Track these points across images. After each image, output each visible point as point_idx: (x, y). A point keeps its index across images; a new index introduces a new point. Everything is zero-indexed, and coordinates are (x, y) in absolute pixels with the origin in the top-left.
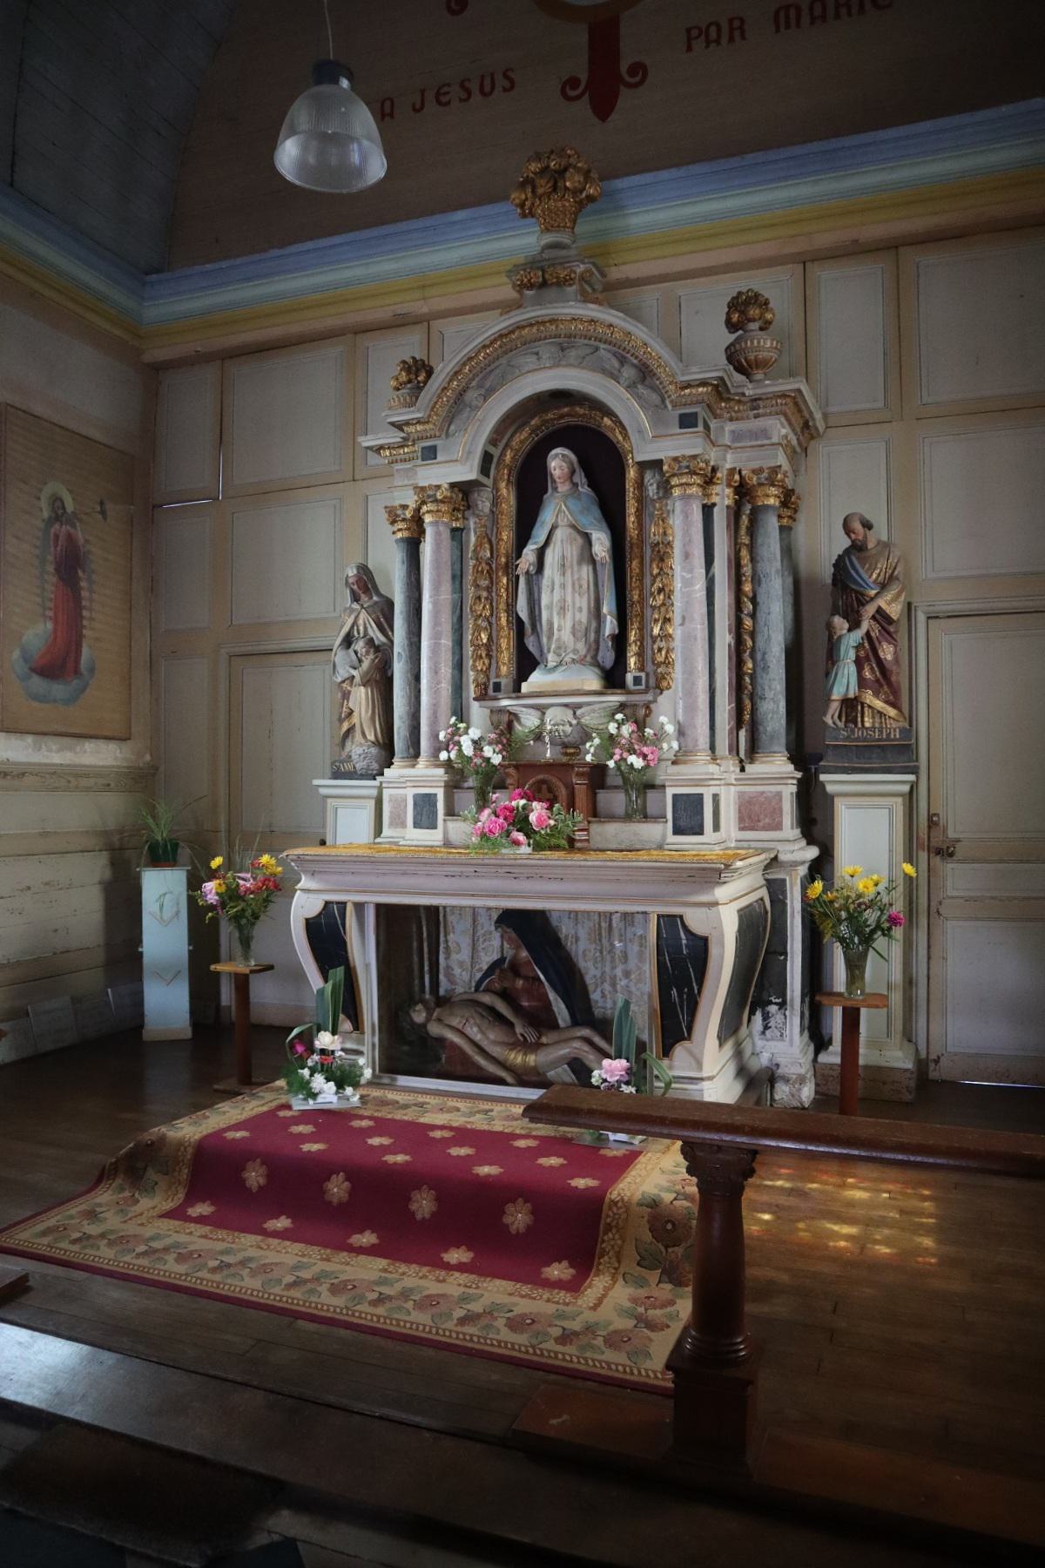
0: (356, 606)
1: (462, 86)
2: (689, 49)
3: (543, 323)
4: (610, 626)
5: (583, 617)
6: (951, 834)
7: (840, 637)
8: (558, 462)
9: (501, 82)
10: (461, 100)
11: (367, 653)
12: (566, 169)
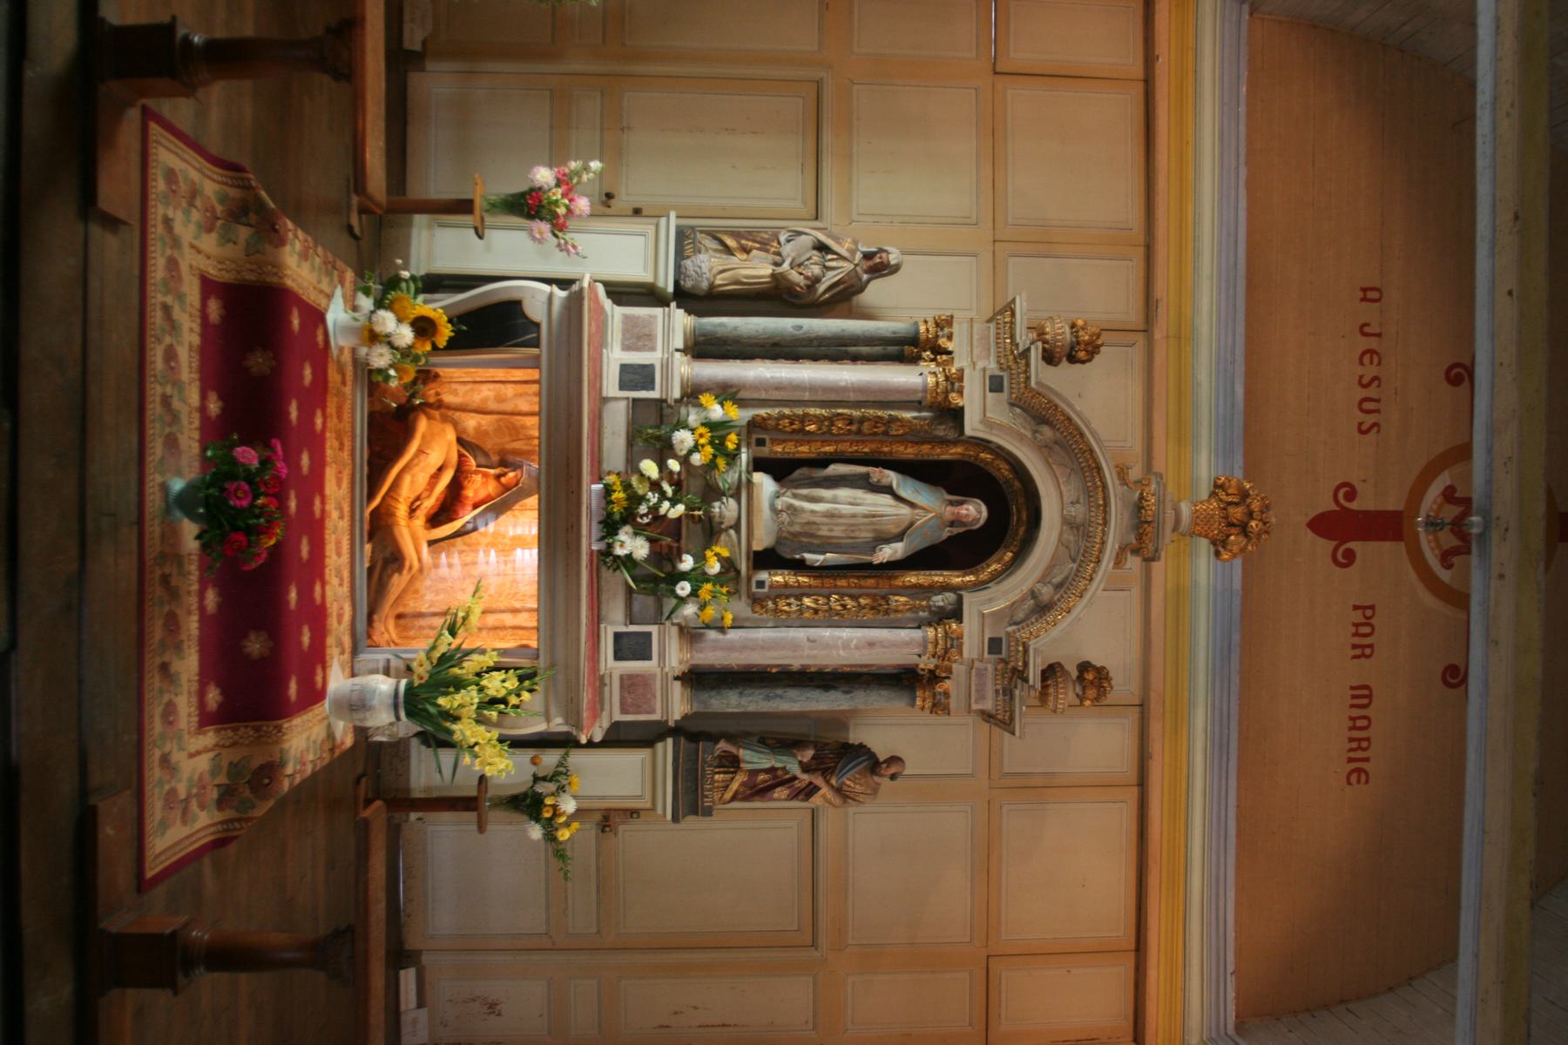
0: (859, 256)
1: (1375, 378)
2: (1356, 608)
3: (1105, 512)
5: (824, 532)
6: (621, 828)
7: (794, 756)
8: (974, 511)
9: (1369, 420)
11: (807, 278)
12: (1246, 536)
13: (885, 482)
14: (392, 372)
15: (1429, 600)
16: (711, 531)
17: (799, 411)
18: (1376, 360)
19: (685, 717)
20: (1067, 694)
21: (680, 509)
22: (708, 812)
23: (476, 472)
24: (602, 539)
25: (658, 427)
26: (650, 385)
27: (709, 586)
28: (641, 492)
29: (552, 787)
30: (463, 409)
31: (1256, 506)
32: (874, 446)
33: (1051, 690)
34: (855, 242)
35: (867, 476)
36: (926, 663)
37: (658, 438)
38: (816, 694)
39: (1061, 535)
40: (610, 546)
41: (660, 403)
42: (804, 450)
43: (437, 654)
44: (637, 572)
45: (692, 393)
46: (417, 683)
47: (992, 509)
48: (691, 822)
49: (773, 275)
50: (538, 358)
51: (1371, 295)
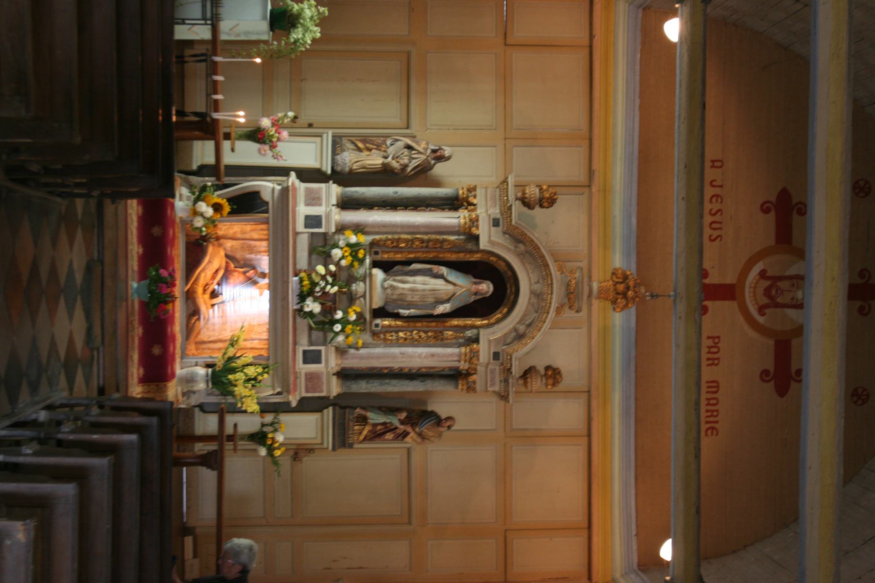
0: (429, 151)
4: (404, 312)
5: (409, 298)
6: (304, 459)
8: (486, 287)
9: (716, 233)
13: (440, 272)
14: (204, 229)
15: (752, 333)
16: (352, 299)
17: (396, 236)
18: (719, 200)
19: (339, 396)
20: (536, 383)
21: (336, 288)
22: (351, 446)
23: (236, 271)
24: (298, 303)
25: (324, 246)
26: (319, 225)
27: (350, 326)
28: (317, 281)
29: (270, 429)
30: (225, 237)
31: (631, 284)
32: (435, 254)
33: (529, 380)
34: (427, 144)
35: (430, 270)
36: (463, 366)
37: (324, 252)
38: (406, 382)
39: (530, 299)
40: (302, 307)
41: (325, 235)
42: (399, 257)
43: (226, 356)
44: (314, 320)
45: (341, 228)
46: (218, 369)
47: (495, 288)
48: (343, 453)
49: (383, 164)
50: (268, 218)
51: (717, 164)
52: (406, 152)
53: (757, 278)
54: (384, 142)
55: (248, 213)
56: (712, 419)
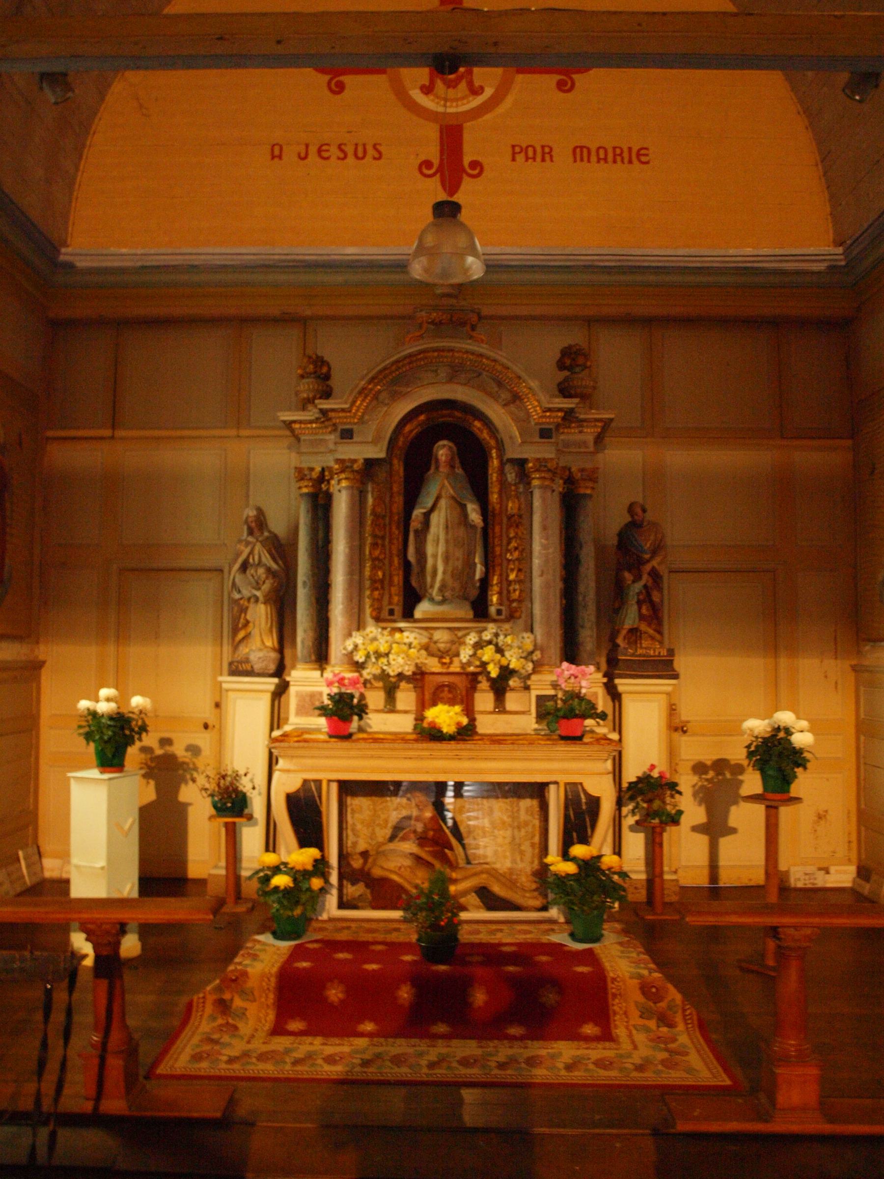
0: (250, 539)
2: (514, 159)
5: (459, 564)
6: (684, 718)
7: (629, 586)
8: (443, 451)
9: (371, 152)
10: (339, 158)
11: (267, 578)
13: (421, 518)
17: (368, 583)
32: (394, 528)
34: (240, 541)
42: (398, 579)
51: (277, 152)
52: (251, 571)
53: (432, 97)
54: (236, 602)
55: (319, 813)
56: (626, 155)
